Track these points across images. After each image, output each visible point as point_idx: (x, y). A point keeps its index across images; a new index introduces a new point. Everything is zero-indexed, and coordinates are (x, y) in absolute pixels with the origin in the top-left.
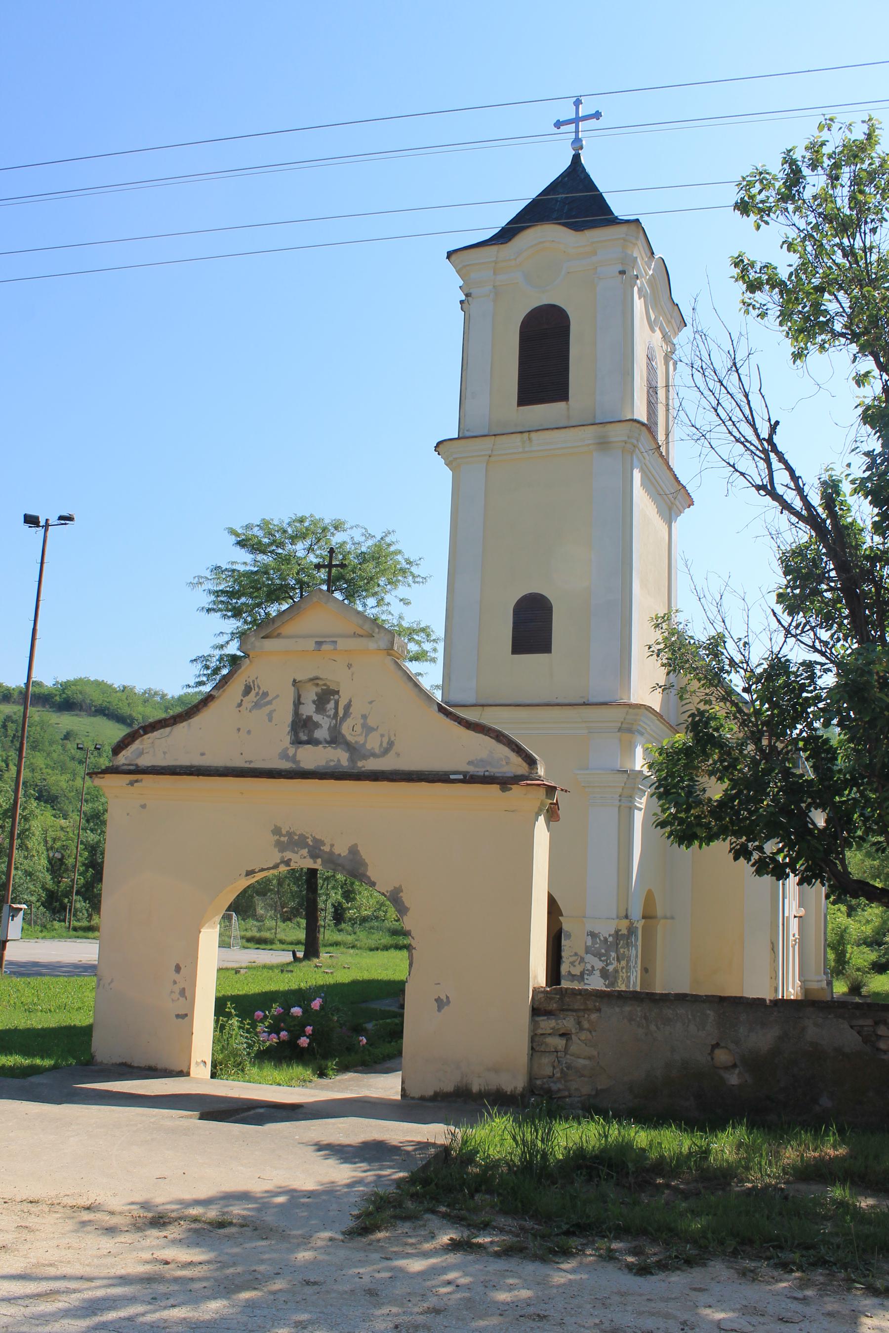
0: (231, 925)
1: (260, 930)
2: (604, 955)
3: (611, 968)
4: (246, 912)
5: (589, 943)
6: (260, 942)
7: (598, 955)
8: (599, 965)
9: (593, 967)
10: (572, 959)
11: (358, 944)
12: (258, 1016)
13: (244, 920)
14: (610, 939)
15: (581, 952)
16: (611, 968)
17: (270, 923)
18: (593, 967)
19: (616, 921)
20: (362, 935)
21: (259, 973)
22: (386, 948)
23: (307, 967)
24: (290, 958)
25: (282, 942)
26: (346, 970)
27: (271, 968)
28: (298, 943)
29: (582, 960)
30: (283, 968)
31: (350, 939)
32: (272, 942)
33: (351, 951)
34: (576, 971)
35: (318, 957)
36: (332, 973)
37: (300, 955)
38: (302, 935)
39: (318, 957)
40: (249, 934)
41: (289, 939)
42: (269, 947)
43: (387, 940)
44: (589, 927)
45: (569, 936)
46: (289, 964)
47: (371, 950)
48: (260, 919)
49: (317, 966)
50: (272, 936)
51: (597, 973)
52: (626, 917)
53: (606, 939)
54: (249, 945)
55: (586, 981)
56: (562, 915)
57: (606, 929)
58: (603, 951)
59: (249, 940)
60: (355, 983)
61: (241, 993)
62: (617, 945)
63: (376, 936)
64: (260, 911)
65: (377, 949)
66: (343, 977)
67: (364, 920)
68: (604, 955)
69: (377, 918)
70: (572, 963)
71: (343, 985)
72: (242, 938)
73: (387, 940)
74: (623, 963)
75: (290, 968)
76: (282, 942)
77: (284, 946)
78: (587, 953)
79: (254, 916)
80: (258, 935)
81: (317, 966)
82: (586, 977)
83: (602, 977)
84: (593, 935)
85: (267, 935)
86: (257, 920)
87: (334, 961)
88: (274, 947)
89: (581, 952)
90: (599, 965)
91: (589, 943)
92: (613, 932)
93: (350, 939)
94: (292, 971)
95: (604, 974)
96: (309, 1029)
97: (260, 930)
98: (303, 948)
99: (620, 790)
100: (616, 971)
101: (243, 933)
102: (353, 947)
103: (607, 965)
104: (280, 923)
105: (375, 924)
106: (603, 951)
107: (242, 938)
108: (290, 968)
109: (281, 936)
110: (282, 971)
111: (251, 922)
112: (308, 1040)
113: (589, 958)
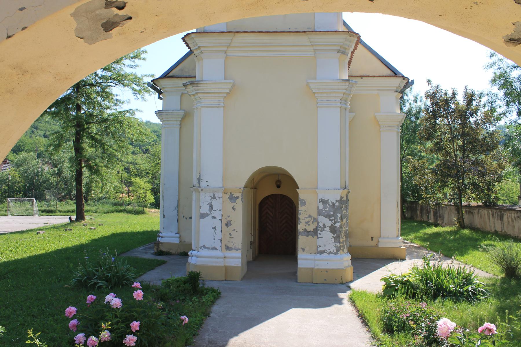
0: (33, 205)
1: (48, 206)
2: (332, 216)
3: (338, 225)
4: (40, 198)
5: (321, 208)
6: (49, 212)
7: (328, 216)
8: (328, 223)
9: (324, 225)
10: (307, 220)
11: (98, 210)
12: (70, 313)
13: (40, 202)
14: (337, 204)
15: (314, 215)
16: (338, 225)
17: (52, 203)
18: (324, 225)
19: (342, 190)
20: (100, 206)
21: (52, 232)
22: (112, 212)
23: (78, 227)
24: (68, 221)
25: (60, 211)
26: (101, 226)
27: (55, 227)
28: (73, 212)
29: (315, 220)
30: (65, 227)
31: (94, 208)
32: (55, 212)
33: (96, 214)
34: (311, 228)
35: (84, 219)
36: (95, 229)
37: (74, 218)
38: (74, 207)
39: (84, 219)
40: (43, 208)
41: (63, 210)
42: (54, 214)
43: (112, 208)
44: (321, 196)
45: (304, 203)
46: (68, 224)
47: (105, 213)
48: (48, 201)
49: (84, 225)
50: (55, 209)
51: (328, 229)
52: (345, 188)
53: (334, 204)
54: (43, 214)
55: (319, 236)
56: (298, 188)
57: (334, 197)
58: (332, 213)
59: (43, 211)
60: (113, 236)
61: (41, 252)
62: (341, 208)
63: (106, 207)
64: (48, 197)
65: (108, 212)
66: (105, 231)
67: (100, 199)
68: (332, 216)
69: (106, 198)
70: (307, 223)
71: (106, 237)
72: (39, 210)
73: (112, 208)
74: (344, 220)
75: (69, 228)
76: (60, 211)
77: (61, 214)
78: (319, 215)
79: (45, 200)
80: (47, 209)
81: (84, 225)
82: (319, 232)
83: (331, 232)
84: (324, 202)
85: (52, 208)
86: (47, 202)
87: (93, 221)
88: (56, 214)
89: (314, 215)
90: (328, 223)
91: (321, 208)
92: (339, 199)
93: (94, 208)
94: (71, 230)
95: (333, 229)
96: (135, 325)
97: (48, 206)
98: (75, 214)
99: (342, 95)
100: (341, 226)
101: (40, 208)
102: (96, 212)
103: (335, 223)
104: (58, 203)
105: (105, 201)
106: (332, 213)
107: (39, 210)
108: (69, 228)
109: (59, 208)
110: (66, 230)
111: (44, 203)
112: (135, 338)
113: (321, 218)
